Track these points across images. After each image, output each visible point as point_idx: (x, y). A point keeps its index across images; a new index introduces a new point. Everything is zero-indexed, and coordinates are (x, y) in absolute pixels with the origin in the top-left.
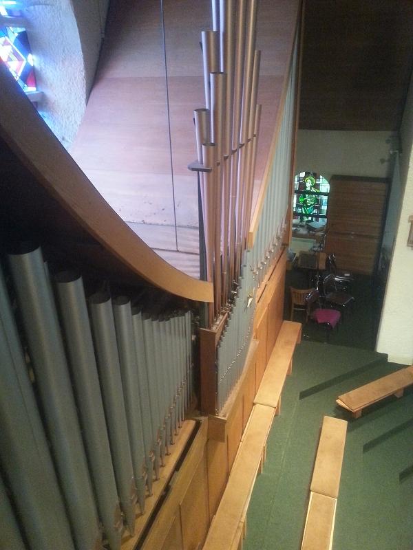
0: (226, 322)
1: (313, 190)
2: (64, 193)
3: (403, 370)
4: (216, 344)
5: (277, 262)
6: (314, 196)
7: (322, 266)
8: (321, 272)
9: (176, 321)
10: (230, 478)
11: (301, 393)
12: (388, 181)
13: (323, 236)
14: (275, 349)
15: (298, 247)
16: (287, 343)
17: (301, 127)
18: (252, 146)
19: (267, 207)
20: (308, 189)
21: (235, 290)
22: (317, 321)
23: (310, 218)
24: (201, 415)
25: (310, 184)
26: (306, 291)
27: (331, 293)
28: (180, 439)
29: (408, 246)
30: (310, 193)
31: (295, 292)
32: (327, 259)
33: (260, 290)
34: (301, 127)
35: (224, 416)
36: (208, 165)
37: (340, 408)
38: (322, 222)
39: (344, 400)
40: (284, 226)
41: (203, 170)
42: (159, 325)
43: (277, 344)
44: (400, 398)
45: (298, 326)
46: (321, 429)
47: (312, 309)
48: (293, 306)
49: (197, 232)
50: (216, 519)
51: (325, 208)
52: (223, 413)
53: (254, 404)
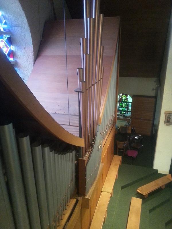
0: (90, 155)
1: (125, 101)
3: (165, 176)
6: (126, 103)
7: (130, 132)
8: (129, 134)
11: (122, 187)
12: (156, 97)
15: (120, 124)
16: (116, 165)
20: (123, 100)
21: (93, 142)
24: (79, 196)
26: (124, 142)
27: (133, 144)
28: (70, 207)
29: (165, 124)
33: (104, 142)
35: (89, 197)
36: (83, 90)
37: (138, 193)
38: (129, 114)
41: (80, 92)
43: (111, 165)
45: (120, 157)
46: (131, 203)
49: (78, 117)
51: (130, 108)
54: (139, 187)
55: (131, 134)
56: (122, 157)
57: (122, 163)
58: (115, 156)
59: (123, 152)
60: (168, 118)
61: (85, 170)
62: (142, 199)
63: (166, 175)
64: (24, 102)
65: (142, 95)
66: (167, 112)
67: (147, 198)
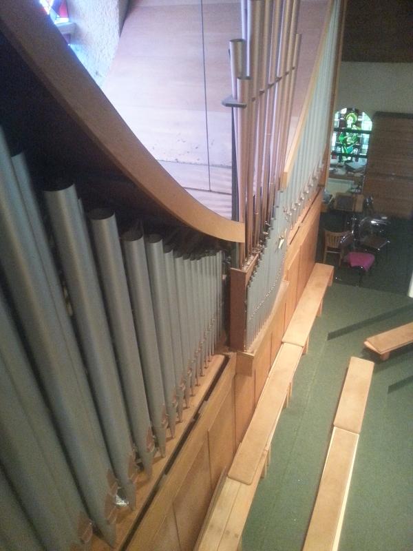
0: (257, 263)
1: (355, 128)
4: (246, 284)
6: (355, 135)
7: (359, 207)
13: (362, 176)
14: (305, 290)
15: (334, 188)
16: (319, 285)
18: (290, 82)
20: (349, 126)
22: (350, 264)
23: (349, 158)
24: (230, 350)
25: (352, 122)
26: (341, 234)
27: (366, 237)
28: (209, 371)
30: (350, 131)
31: (328, 235)
33: (293, 231)
34: (342, 60)
35: (252, 352)
36: (243, 99)
37: (367, 350)
38: (361, 162)
41: (237, 106)
43: (308, 286)
45: (329, 269)
46: (347, 369)
48: (326, 249)
49: (230, 171)
51: (365, 147)
52: (251, 350)
53: (282, 343)
56: (335, 269)
67: (386, 361)
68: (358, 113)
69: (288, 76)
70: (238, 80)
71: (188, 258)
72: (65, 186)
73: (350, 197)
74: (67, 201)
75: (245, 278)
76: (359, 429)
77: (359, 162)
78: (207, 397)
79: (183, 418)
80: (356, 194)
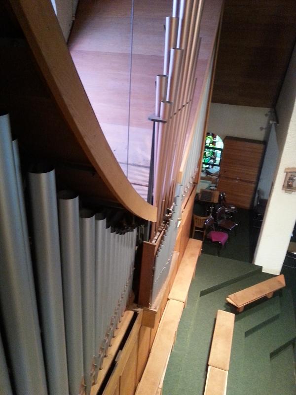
0: (162, 238)
1: (211, 146)
2: (82, 127)
3: (274, 278)
4: (155, 253)
5: (190, 196)
6: (211, 150)
7: (216, 200)
8: (214, 205)
9: (123, 237)
10: (151, 354)
11: (201, 292)
12: (265, 143)
13: (217, 179)
14: (183, 259)
15: (203, 185)
16: (192, 255)
17: (213, 101)
18: (185, 111)
19: (192, 156)
20: (208, 145)
21: (168, 214)
22: (211, 240)
23: (207, 166)
24: (138, 307)
25: (209, 142)
26: (205, 218)
27: (221, 221)
28: (122, 324)
29: (283, 189)
30: (208, 148)
31: (196, 218)
32: (220, 196)
33: (181, 213)
34: (213, 101)
35: (155, 309)
36: (164, 117)
37: (229, 304)
38: (216, 169)
39: (232, 299)
40: (197, 170)
41: (159, 121)
42: (118, 238)
43: (185, 255)
44: (271, 298)
45: (199, 243)
46: (215, 320)
47: (208, 231)
48: (194, 228)
49: (148, 171)
50: (140, 385)
51: (218, 159)
52: (154, 306)
53: (168, 299)
54: (229, 295)
55: (217, 204)
56: (203, 243)
57: (203, 252)
58: (192, 241)
59: (203, 233)
60: (291, 179)
61: (153, 261)
62: (236, 315)
63: (275, 276)
64: (81, 128)
65: (241, 137)
66: (289, 168)
67: (242, 312)
68: (214, 136)
69: (184, 108)
70: (162, 103)
71: (114, 232)
72: (47, 170)
73: (210, 193)
74: (47, 181)
75: (154, 249)
76: (228, 368)
77: (214, 169)
78: (121, 347)
79: (103, 367)
80: (213, 190)
